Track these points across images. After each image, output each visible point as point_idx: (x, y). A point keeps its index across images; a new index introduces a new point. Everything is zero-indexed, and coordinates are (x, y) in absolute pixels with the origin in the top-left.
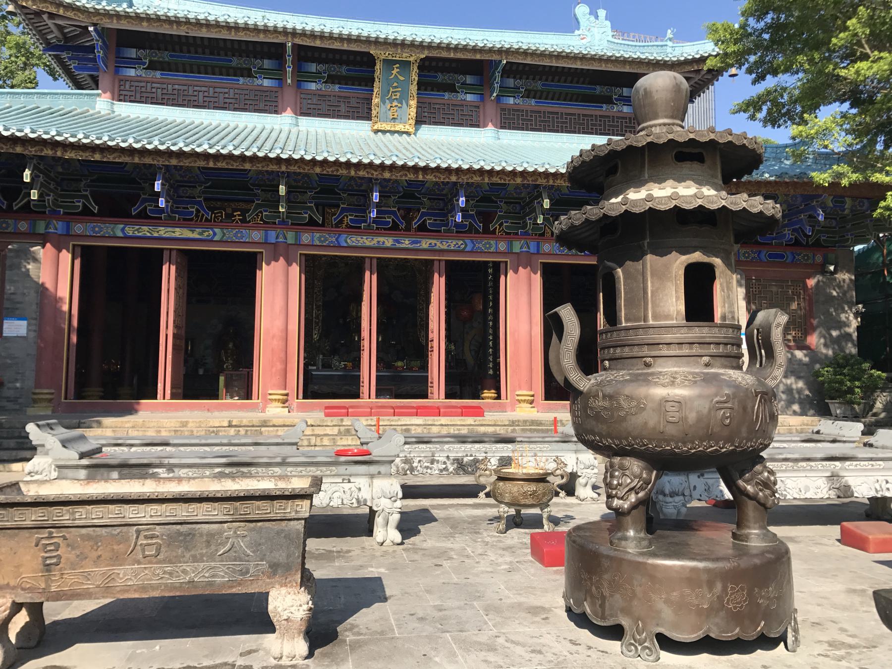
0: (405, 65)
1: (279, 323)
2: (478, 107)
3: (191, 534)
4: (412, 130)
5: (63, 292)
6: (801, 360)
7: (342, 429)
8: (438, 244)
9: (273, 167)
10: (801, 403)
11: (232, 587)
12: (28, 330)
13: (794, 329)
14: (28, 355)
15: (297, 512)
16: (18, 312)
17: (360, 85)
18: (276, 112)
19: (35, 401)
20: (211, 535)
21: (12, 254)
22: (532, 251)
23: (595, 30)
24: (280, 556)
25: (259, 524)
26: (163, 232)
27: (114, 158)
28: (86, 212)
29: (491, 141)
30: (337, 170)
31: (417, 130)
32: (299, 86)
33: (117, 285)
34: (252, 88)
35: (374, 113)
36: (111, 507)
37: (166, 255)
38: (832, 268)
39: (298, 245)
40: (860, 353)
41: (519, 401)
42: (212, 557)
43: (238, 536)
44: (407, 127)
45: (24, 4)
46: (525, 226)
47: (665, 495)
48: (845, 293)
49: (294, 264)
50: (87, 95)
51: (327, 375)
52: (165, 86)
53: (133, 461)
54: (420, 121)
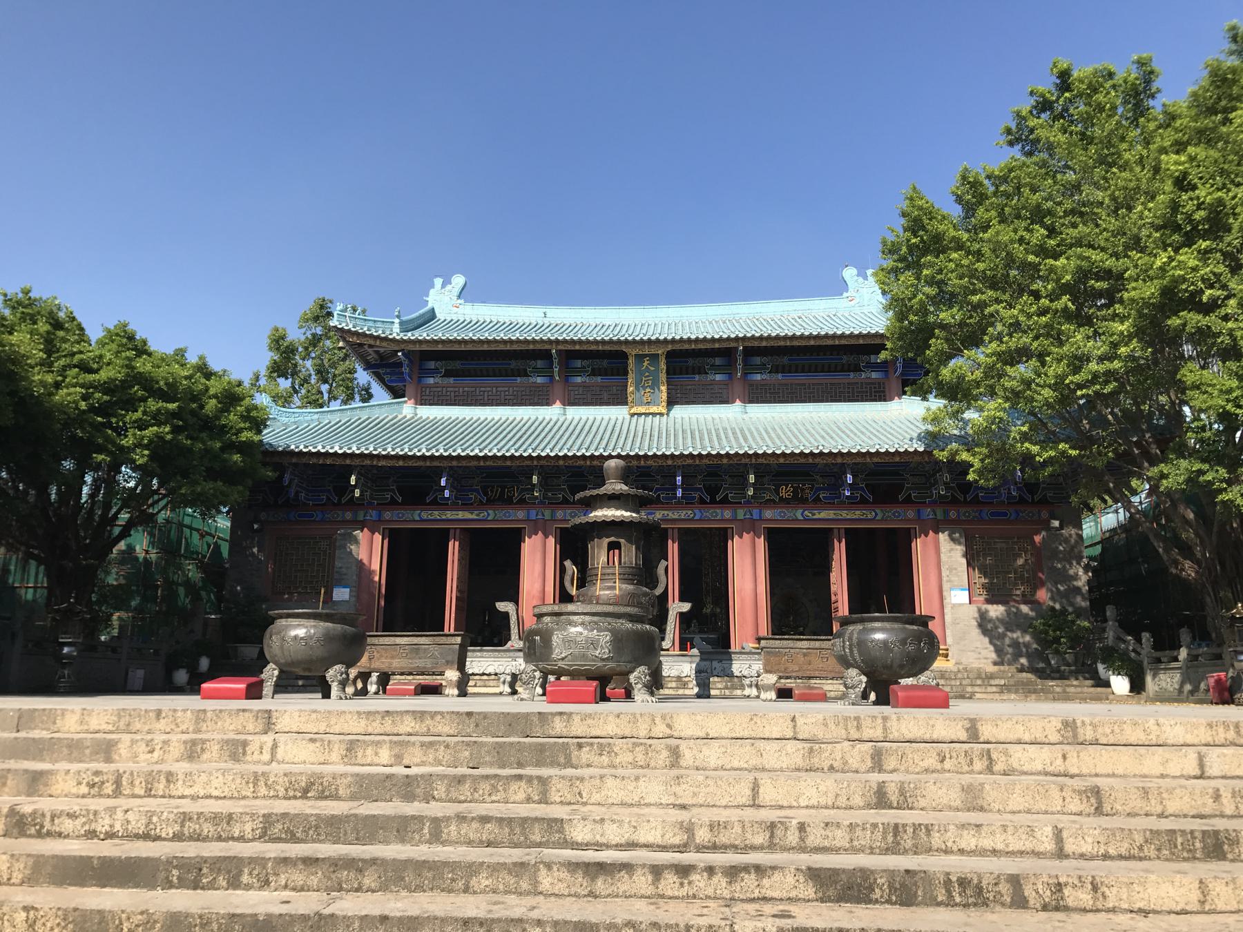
0: (654, 357)
1: (537, 586)
4: (664, 411)
5: (375, 566)
6: (1027, 615)
10: (1028, 656)
13: (1022, 584)
24: (450, 658)
26: (449, 515)
28: (393, 503)
31: (669, 411)
32: (419, 381)
33: (415, 559)
35: (630, 399)
37: (452, 532)
38: (1056, 523)
39: (554, 520)
54: (671, 403)
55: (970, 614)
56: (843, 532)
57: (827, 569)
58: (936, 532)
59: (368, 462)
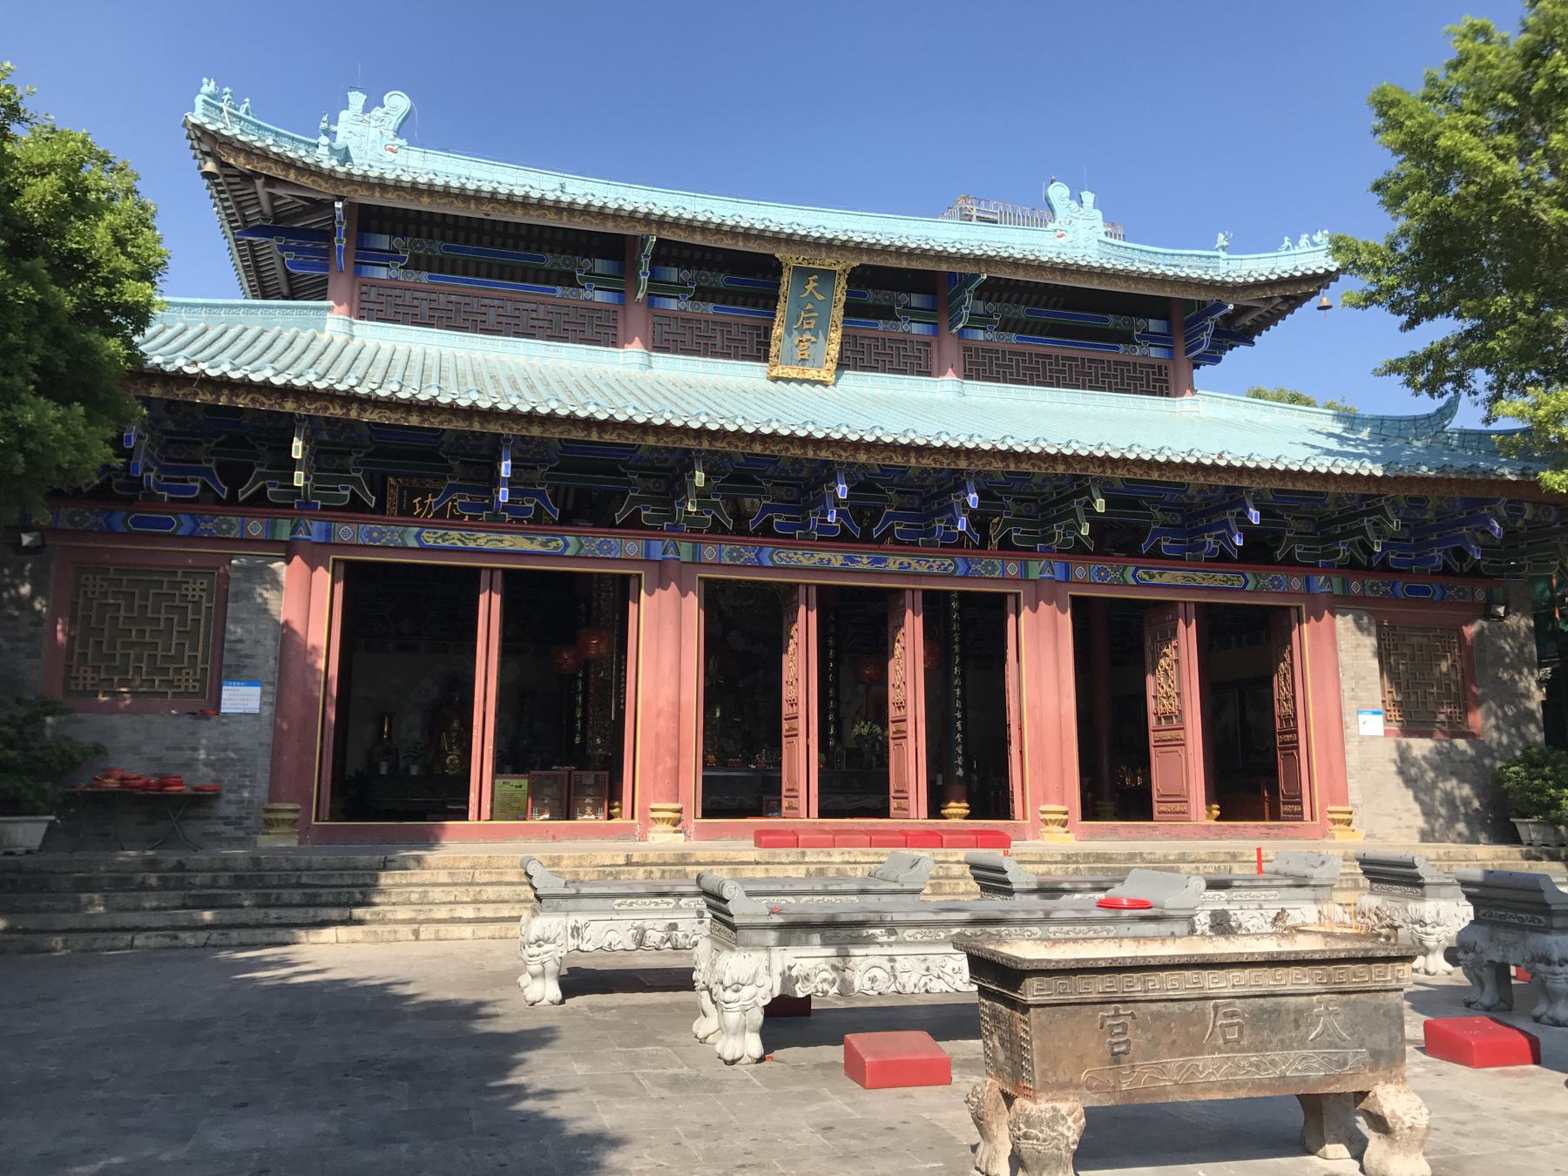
0: (828, 276)
1: (668, 691)
2: (928, 344)
3: (1276, 1011)
4: (830, 378)
7: (813, 868)
8: (914, 564)
9: (689, 443)
11: (1328, 1085)
12: (263, 703)
14: (261, 745)
15: (1398, 980)
16: (245, 672)
17: (744, 305)
18: (614, 344)
19: (269, 824)
20: (1299, 1011)
21: (238, 575)
22: (1057, 577)
23: (1079, 224)
25: (1353, 996)
26: (483, 540)
27: (441, 423)
28: (356, 507)
29: (635, 372)
30: (787, 449)
31: (837, 379)
32: (357, 272)
34: (575, 304)
35: (773, 350)
36: (1187, 973)
38: (1501, 610)
39: (697, 563)
40: (1548, 740)
41: (1046, 822)
42: (1303, 1043)
43: (1330, 1013)
44: (823, 373)
45: (231, 161)
46: (805, 526)
47: (1549, 962)
48: (1521, 647)
49: (691, 594)
50: (314, 308)
51: (738, 780)
52: (434, 296)
53: (843, 918)
54: (842, 366)
55: (1387, 750)
56: (1192, 609)
57: (778, 646)
58: (1333, 615)
59: (336, 411)
